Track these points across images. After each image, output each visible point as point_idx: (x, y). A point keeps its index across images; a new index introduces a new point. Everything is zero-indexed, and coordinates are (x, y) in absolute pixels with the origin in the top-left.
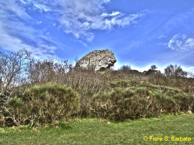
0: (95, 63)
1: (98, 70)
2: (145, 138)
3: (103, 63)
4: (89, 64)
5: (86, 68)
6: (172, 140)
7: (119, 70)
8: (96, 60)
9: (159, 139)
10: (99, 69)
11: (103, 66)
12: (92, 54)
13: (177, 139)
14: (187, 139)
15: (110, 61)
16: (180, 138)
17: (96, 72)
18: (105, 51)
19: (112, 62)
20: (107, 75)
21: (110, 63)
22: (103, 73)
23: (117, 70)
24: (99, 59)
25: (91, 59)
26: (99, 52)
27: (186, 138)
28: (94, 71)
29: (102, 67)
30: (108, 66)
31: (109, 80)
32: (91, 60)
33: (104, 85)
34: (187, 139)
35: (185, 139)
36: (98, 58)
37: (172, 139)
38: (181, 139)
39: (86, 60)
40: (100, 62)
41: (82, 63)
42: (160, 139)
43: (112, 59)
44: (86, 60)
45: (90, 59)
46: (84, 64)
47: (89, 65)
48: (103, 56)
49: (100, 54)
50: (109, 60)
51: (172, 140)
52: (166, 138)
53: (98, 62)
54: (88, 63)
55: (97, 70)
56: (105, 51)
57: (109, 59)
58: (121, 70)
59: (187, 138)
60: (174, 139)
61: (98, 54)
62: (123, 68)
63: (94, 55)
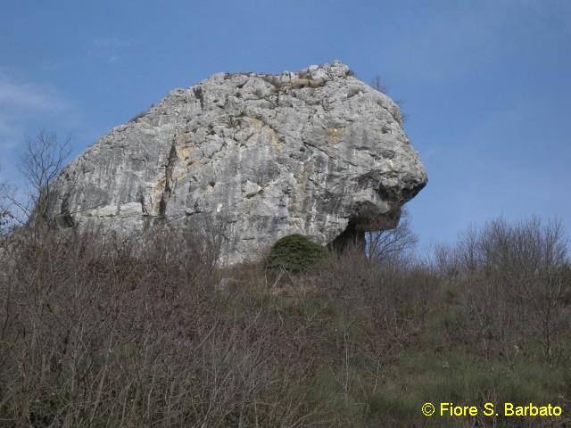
0: (223, 196)
1: (246, 266)
2: (427, 409)
3: (300, 197)
4: (162, 206)
5: (129, 242)
6: (506, 414)
7: (453, 272)
8: (234, 166)
9: (468, 411)
10: (254, 258)
11: (296, 226)
12: (194, 108)
13: (522, 410)
14: (552, 411)
15: (363, 180)
16: (531, 409)
17: (234, 287)
18: (323, 83)
19: (383, 192)
20: (329, 312)
21: (367, 194)
22: (302, 287)
23: (435, 264)
24: (265, 154)
25: (182, 154)
26: (258, 94)
27: (547, 406)
28: (211, 269)
29: (284, 231)
30: (343, 223)
31: (356, 362)
32: (179, 170)
33: (302, 411)
34: (552, 411)
35: (546, 410)
36: (251, 144)
37: (506, 409)
38: (534, 411)
39: (136, 163)
40: (273, 189)
41: (92, 190)
42: (470, 411)
43: (384, 165)
44: (136, 163)
45: (172, 156)
46: (111, 208)
47: (162, 216)
48: (295, 135)
49: (267, 112)
50: (361, 171)
51: (506, 414)
52: (489, 406)
53: (251, 187)
54: (153, 197)
55: (237, 259)
56: (323, 83)
57: (359, 156)
58: (472, 266)
59: (550, 407)
60: (511, 409)
61: (254, 107)
62: (486, 247)
63: (212, 116)
